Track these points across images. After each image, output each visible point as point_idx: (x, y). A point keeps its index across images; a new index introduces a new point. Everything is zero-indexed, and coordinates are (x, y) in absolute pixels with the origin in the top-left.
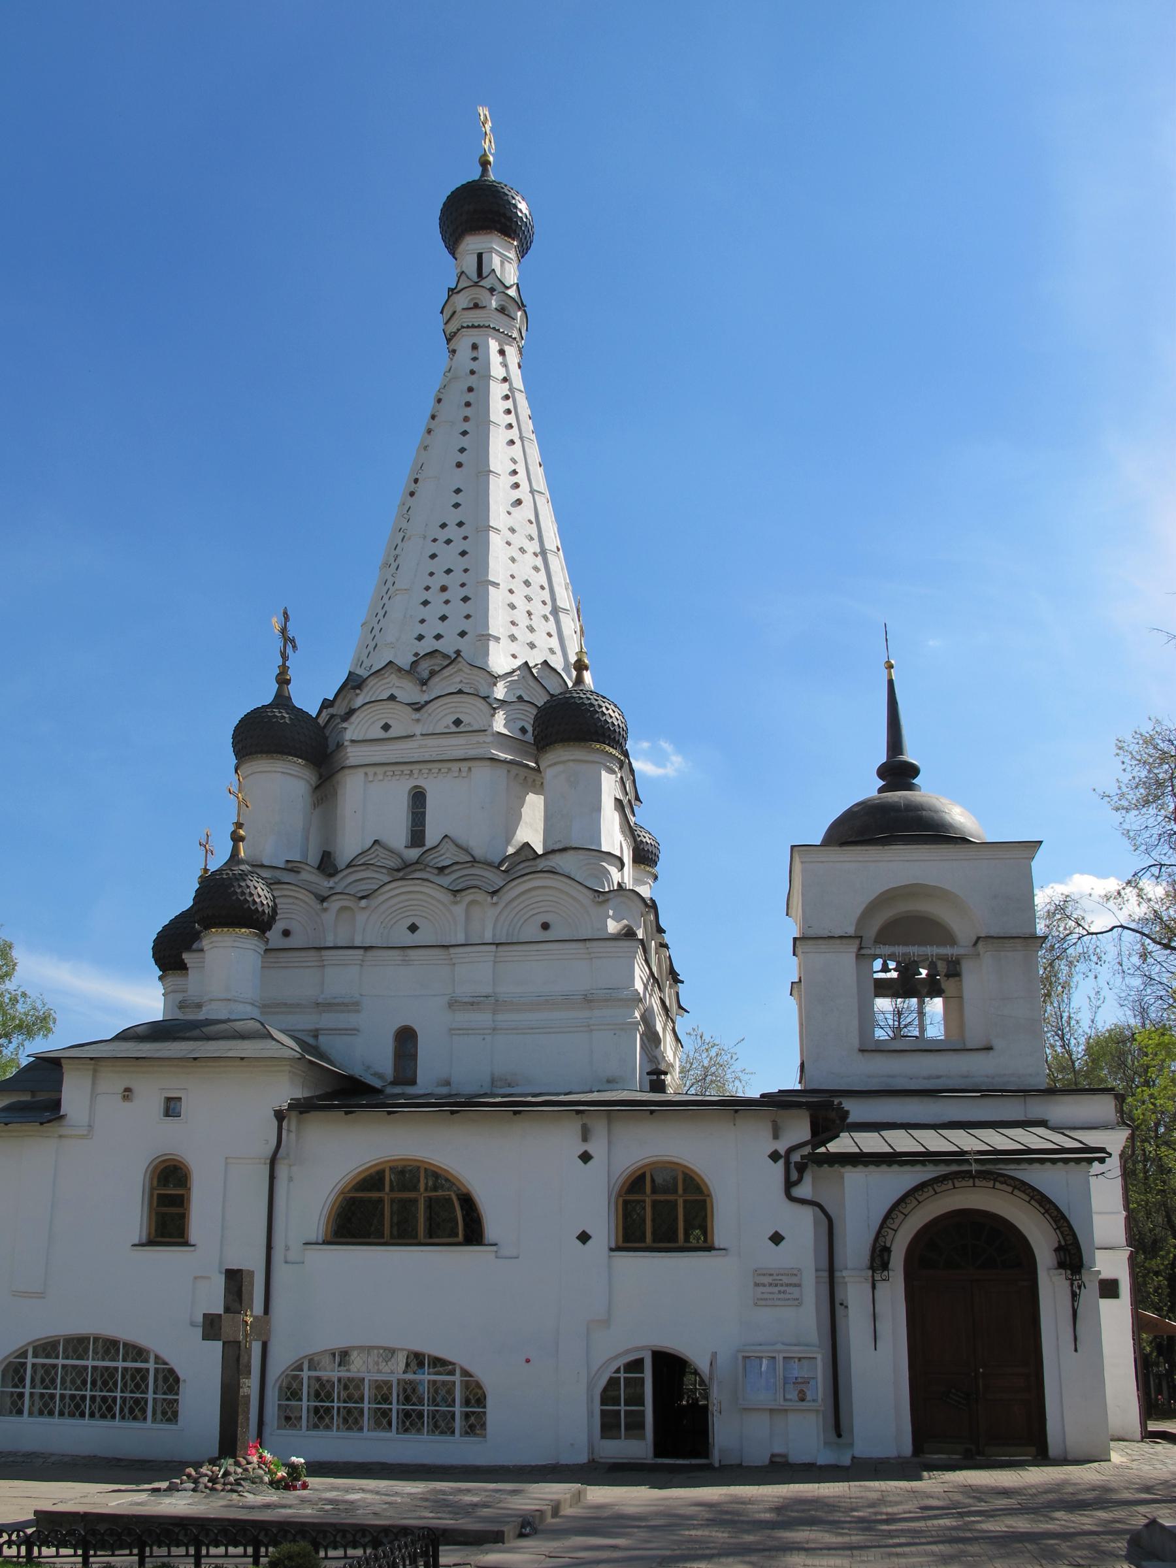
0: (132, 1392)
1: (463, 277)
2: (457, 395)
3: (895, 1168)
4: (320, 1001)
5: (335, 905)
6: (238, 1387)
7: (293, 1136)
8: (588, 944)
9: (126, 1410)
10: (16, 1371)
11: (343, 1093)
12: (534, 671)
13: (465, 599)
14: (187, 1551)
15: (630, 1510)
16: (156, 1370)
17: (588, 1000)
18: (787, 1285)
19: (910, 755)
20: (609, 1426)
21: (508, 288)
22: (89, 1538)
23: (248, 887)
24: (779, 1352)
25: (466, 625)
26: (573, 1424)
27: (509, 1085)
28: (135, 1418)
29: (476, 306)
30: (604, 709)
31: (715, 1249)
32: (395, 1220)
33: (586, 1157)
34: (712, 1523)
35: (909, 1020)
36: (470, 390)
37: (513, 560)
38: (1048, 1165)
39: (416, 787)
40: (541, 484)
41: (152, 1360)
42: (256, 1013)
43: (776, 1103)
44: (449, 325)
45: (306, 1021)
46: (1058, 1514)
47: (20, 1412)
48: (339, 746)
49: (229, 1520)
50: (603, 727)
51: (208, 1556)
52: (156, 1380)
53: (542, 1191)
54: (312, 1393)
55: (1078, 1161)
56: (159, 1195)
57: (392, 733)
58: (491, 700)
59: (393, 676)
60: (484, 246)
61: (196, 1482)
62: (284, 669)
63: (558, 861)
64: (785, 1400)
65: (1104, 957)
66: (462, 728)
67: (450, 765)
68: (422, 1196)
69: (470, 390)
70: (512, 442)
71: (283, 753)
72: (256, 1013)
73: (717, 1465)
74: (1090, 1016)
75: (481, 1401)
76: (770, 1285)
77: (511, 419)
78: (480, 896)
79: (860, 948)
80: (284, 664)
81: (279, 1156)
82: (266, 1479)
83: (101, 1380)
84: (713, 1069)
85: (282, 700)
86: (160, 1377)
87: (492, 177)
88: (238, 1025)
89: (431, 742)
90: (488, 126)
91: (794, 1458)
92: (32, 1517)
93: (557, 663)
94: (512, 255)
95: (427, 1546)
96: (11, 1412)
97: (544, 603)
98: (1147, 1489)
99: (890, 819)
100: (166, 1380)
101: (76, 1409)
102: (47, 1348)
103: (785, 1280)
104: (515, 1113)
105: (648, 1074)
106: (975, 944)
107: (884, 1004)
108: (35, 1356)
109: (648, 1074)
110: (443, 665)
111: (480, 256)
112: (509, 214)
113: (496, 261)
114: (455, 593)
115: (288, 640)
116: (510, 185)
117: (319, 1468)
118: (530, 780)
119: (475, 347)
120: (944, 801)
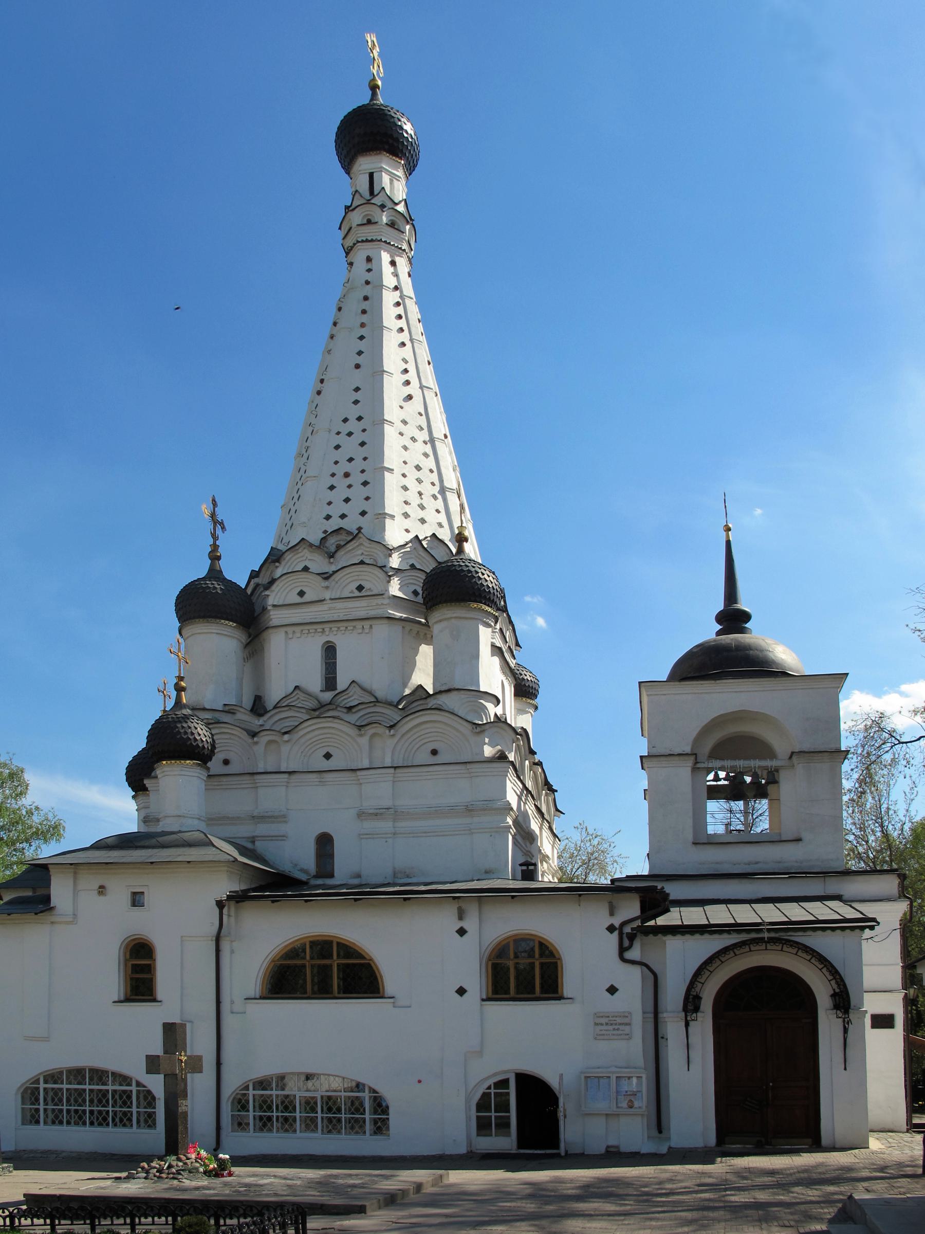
0: (121, 1107)
1: (357, 196)
2: (354, 305)
3: (707, 936)
4: (255, 814)
5: (264, 739)
6: (177, 1106)
7: (232, 919)
8: (468, 766)
9: (117, 1120)
10: (33, 1093)
11: (273, 885)
12: (424, 543)
13: (365, 484)
14: (5, 1222)
15: (472, 1188)
16: (138, 1092)
17: (469, 810)
18: (620, 1024)
19: (743, 604)
20: (483, 1126)
21: (397, 204)
22: (54, 1213)
23: (190, 728)
24: (613, 1073)
25: (365, 506)
26: (455, 1126)
27: (408, 877)
28: (124, 1125)
29: (369, 222)
30: (480, 574)
31: (564, 998)
32: (316, 980)
33: (462, 932)
34: (531, 1197)
35: (760, 812)
36: (366, 298)
37: (405, 448)
38: (829, 931)
39: (328, 642)
40: (430, 380)
41: (134, 1083)
42: (203, 826)
43: (619, 887)
44: (346, 240)
45: (243, 831)
46: (796, 1189)
47: (37, 1122)
48: (264, 609)
49: (165, 1199)
50: (479, 589)
51: (140, 1224)
52: (138, 1098)
53: (427, 959)
54: (257, 1104)
55: (852, 929)
56: (133, 965)
57: (307, 598)
58: (387, 569)
59: (306, 551)
60: (372, 166)
61: (147, 1172)
62: (215, 547)
63: (444, 700)
64: (617, 1107)
65: (912, 762)
66: (363, 593)
67: (354, 624)
68: (335, 962)
69: (366, 298)
70: (403, 344)
71: (216, 617)
72: (203, 826)
73: (563, 1154)
74: (905, 806)
75: (385, 1110)
76: (607, 1024)
77: (402, 323)
78: (380, 730)
79: (696, 763)
80: (215, 544)
81: (222, 934)
82: (201, 1170)
83: (76, 1100)
84: (596, 854)
85: (215, 573)
86: (141, 1096)
87: (381, 100)
88: (186, 836)
89: (339, 605)
90: (376, 53)
91: (623, 1149)
92: (22, 1198)
93: (445, 535)
94: (400, 173)
95: (296, 1217)
96: (31, 1122)
97: (433, 484)
98: (882, 1169)
99: (726, 658)
100: (145, 1098)
101: (79, 1119)
102: (53, 1077)
103: (619, 1020)
104: (405, 899)
105: (521, 865)
106: (791, 757)
107: (713, 806)
108: (46, 1082)
109: (521, 865)
110: (347, 541)
111: (371, 175)
112: (395, 136)
113: (386, 179)
115: (216, 521)
116: (396, 108)
117: (238, 1161)
118: (422, 634)
119: (369, 259)
120: (769, 641)
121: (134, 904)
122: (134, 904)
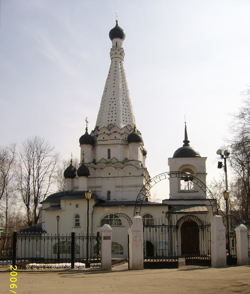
5: (97, 170)
11: (100, 203)
43: (164, 204)
45: (94, 189)
57: (105, 139)
114: (114, 112)
121: (70, 205)
122: (70, 205)
